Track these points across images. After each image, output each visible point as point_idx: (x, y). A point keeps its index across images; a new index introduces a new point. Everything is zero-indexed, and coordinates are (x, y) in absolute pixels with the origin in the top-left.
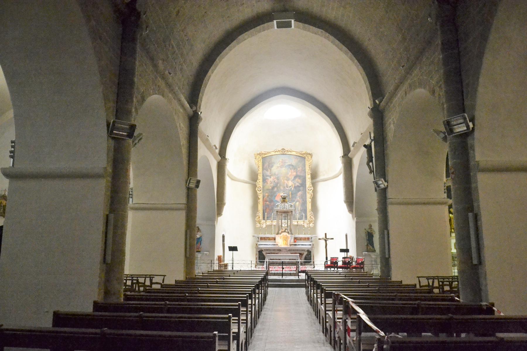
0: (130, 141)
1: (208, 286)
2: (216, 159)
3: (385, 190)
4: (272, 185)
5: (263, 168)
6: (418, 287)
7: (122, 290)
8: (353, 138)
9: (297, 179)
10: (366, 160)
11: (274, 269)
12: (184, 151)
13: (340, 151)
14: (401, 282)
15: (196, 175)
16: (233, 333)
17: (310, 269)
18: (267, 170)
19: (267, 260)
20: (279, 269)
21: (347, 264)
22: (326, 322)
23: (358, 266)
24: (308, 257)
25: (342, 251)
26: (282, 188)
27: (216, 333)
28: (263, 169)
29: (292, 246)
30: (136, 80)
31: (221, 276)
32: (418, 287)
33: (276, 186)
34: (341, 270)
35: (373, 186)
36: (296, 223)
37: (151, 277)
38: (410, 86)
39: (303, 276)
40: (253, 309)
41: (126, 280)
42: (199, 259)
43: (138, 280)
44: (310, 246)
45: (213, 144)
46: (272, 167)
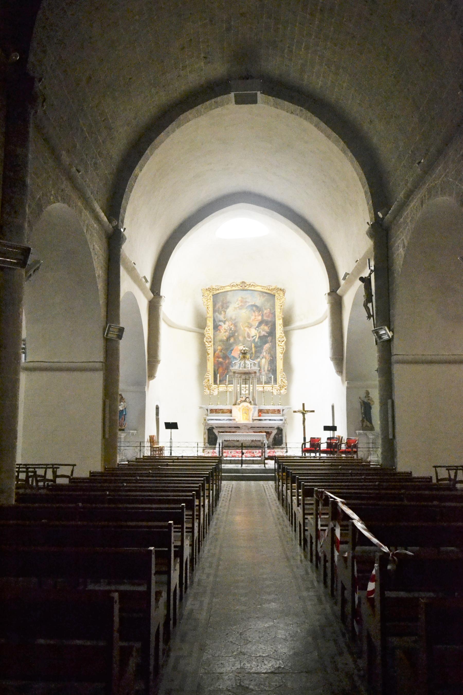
0: (23, 272)
1: (137, 480)
2: (146, 297)
3: (390, 341)
4: (227, 333)
5: (213, 310)
6: (434, 481)
7: (14, 487)
8: (344, 266)
9: (263, 326)
10: (362, 299)
11: (230, 454)
12: (101, 285)
13: (326, 288)
14: (411, 473)
15: (118, 322)
16: (175, 547)
17: (281, 454)
18: (220, 313)
19: (219, 441)
20: (237, 455)
21: (333, 446)
22: (305, 530)
23: (350, 450)
24: (278, 440)
25: (326, 428)
26: (241, 338)
27: (152, 548)
28: (214, 311)
29: (255, 422)
30: (29, 181)
31: (156, 466)
32: (434, 481)
33: (233, 335)
34: (325, 455)
35: (374, 337)
36: (261, 389)
37: (54, 467)
38: (429, 191)
39: (271, 464)
40: (202, 513)
41: (18, 472)
42: (122, 440)
43: (35, 472)
44: (281, 422)
45: (142, 275)
46: (227, 307)
